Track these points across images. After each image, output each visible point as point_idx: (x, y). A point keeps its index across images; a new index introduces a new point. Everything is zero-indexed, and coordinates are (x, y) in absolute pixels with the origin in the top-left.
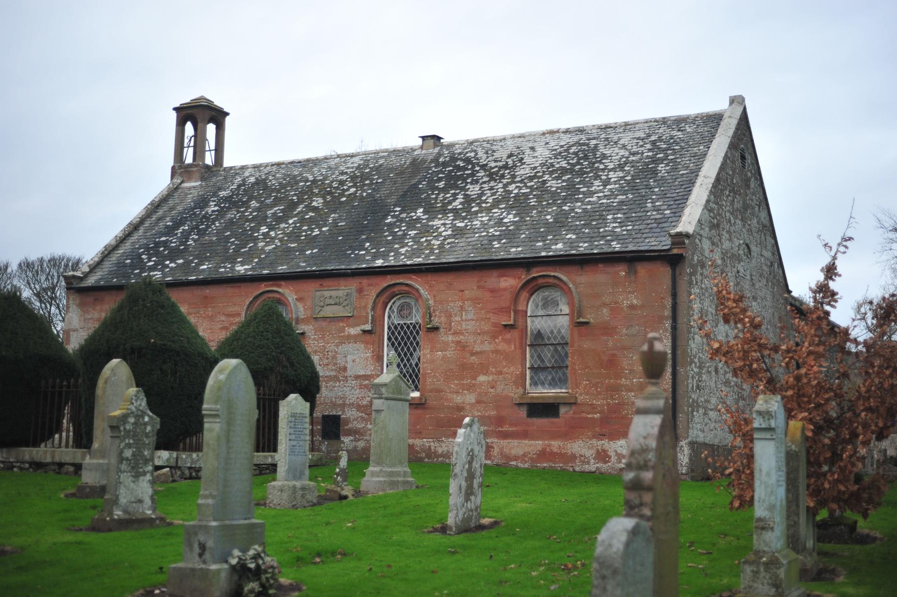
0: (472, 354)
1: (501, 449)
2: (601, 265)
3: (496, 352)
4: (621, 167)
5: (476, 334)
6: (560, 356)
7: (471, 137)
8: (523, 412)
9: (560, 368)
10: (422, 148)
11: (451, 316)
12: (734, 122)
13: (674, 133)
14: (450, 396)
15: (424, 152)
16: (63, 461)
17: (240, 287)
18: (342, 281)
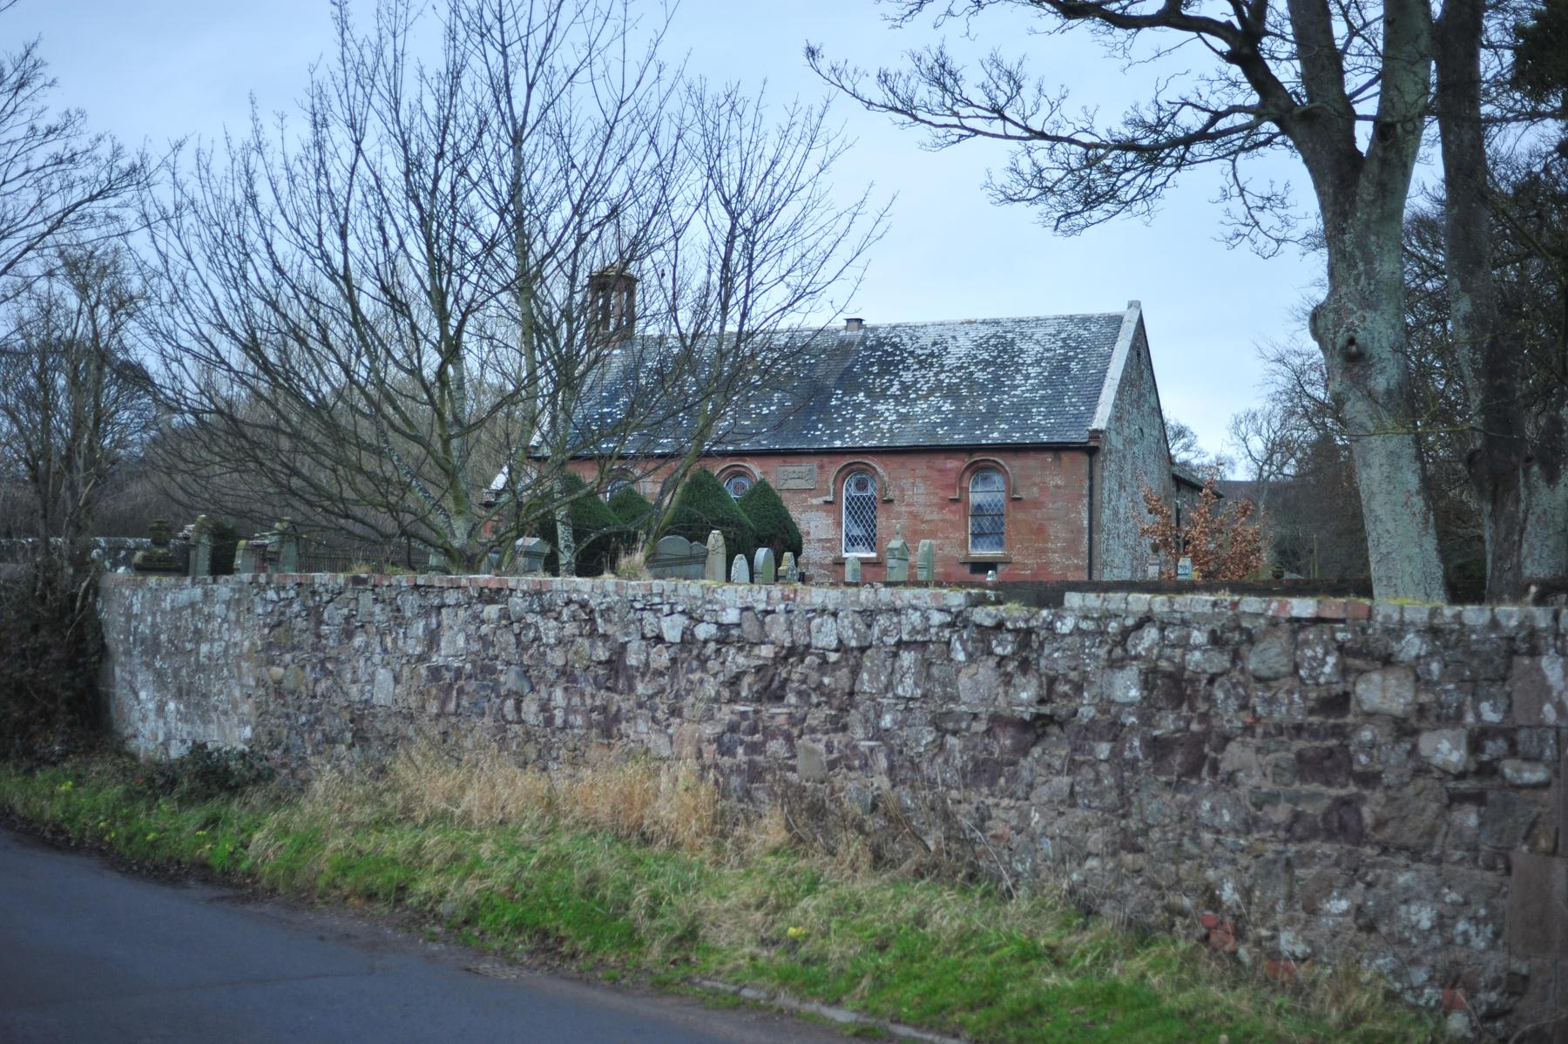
3: (943, 520)
4: (1038, 362)
5: (925, 505)
7: (894, 322)
8: (967, 569)
10: (846, 328)
12: (1133, 326)
13: (1081, 332)
18: (805, 459)
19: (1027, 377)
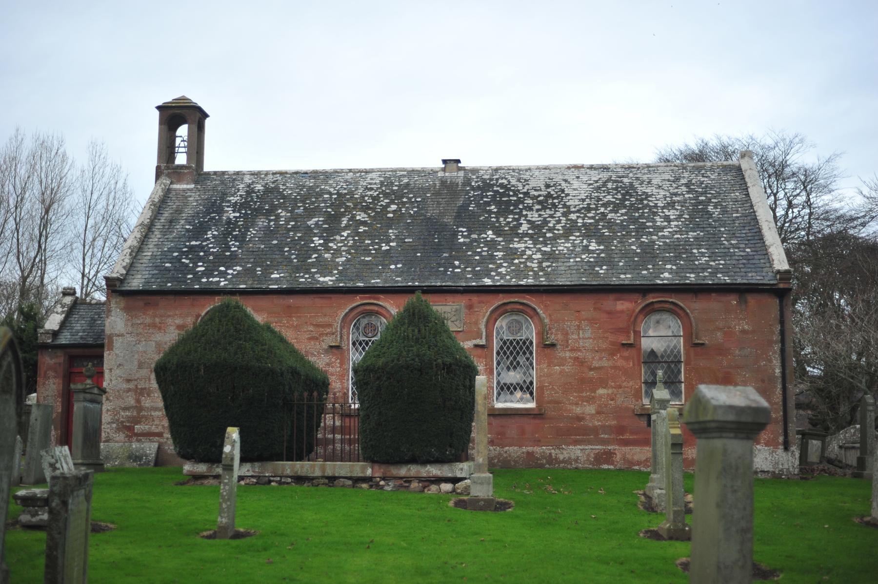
0: (591, 369)
1: (624, 455)
2: (713, 295)
3: (615, 368)
6: (673, 371)
7: (495, 164)
9: (673, 383)
10: (444, 170)
11: (567, 334)
14: (569, 407)
15: (447, 174)
16: (337, 475)
17: (331, 298)
18: (449, 298)
19: (667, 219)
